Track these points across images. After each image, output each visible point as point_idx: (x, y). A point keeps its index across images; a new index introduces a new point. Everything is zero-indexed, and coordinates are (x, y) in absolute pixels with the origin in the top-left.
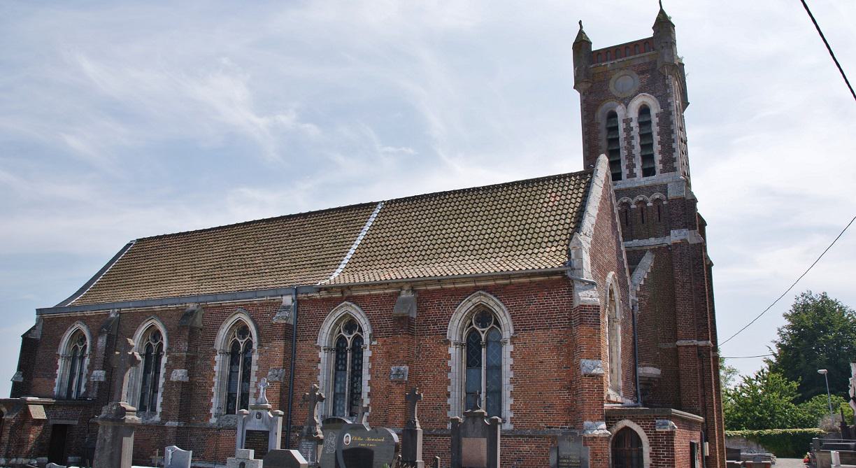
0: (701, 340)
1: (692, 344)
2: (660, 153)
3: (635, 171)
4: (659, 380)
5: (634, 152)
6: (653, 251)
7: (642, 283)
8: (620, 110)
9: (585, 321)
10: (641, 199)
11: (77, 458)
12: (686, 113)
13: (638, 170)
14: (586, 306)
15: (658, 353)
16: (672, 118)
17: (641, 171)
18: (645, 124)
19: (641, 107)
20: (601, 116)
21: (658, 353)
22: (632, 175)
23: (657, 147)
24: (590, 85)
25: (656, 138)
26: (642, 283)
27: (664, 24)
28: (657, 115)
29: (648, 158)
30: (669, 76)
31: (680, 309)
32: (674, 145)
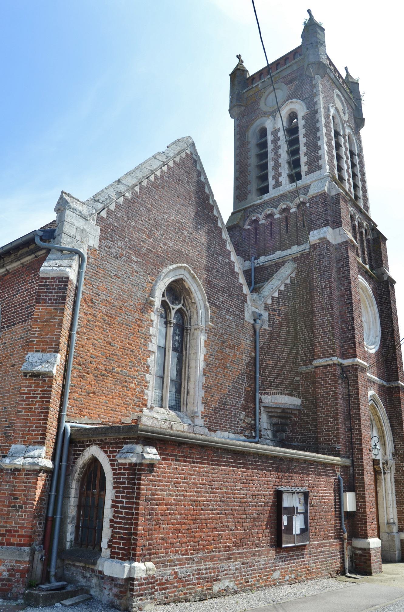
0: (348, 358)
1: (331, 363)
2: (306, 154)
3: (281, 179)
4: (299, 411)
5: (280, 161)
6: (295, 260)
7: (276, 295)
8: (269, 124)
9: (42, 299)
10: (284, 206)
11: (19, 462)
12: (362, 131)
13: (284, 179)
14: (48, 278)
15: (297, 379)
16: (317, 116)
17: (288, 179)
18: (292, 131)
19: (289, 115)
20: (252, 139)
21: (297, 379)
22: (278, 184)
23: (303, 149)
24: (243, 108)
25: (302, 140)
26: (276, 295)
27: (312, 31)
28: (303, 118)
29: (295, 164)
30: (316, 76)
31: (318, 321)
32: (319, 143)
